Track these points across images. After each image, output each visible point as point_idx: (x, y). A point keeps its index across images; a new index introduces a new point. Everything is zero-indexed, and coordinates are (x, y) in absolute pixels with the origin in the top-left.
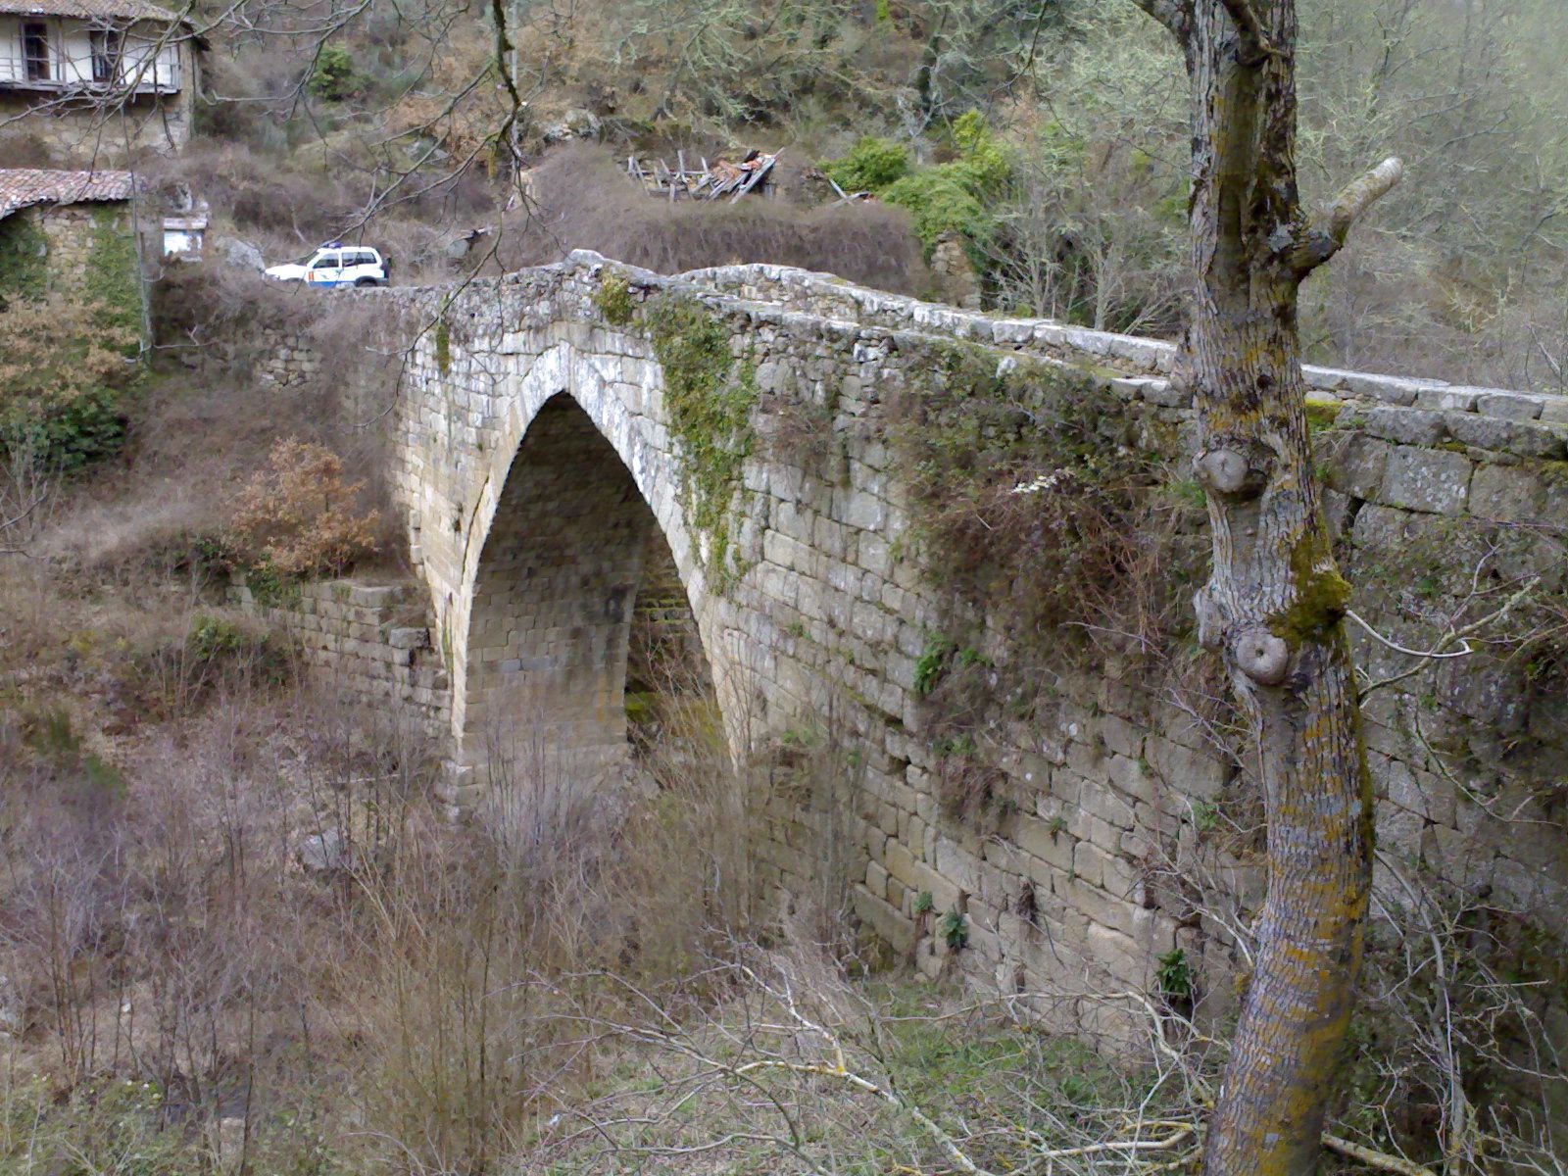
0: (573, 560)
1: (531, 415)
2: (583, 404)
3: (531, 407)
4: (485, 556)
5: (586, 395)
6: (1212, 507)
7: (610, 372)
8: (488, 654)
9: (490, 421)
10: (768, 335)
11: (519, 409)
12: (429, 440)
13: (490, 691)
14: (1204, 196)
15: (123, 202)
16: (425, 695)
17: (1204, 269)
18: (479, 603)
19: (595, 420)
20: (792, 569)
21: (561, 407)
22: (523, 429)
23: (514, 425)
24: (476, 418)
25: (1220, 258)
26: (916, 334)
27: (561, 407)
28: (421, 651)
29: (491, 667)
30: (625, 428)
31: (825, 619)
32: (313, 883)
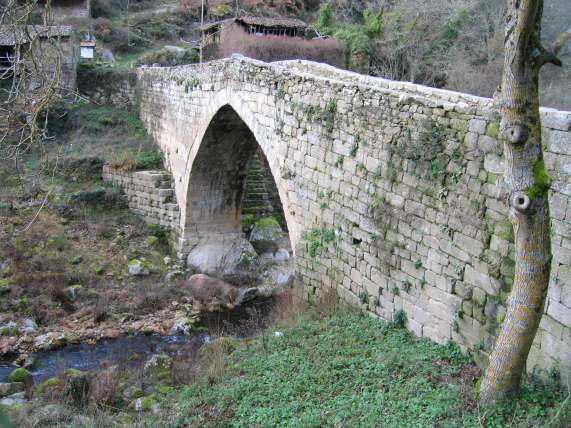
0: (225, 165)
1: (215, 113)
2: (235, 108)
3: (214, 110)
4: (194, 164)
5: (236, 107)
6: (505, 146)
7: (246, 97)
8: (196, 199)
9: (198, 114)
10: (308, 84)
11: (209, 111)
12: (174, 120)
13: (194, 213)
14: (511, 37)
15: (68, 37)
16: (171, 213)
17: (511, 61)
18: (193, 180)
19: (240, 115)
20: (316, 169)
21: (226, 111)
22: (211, 118)
23: (208, 116)
24: (193, 114)
25: (517, 59)
26: (141, 58)
27: (226, 111)
28: (170, 198)
29: (195, 203)
30: (251, 117)
31: (504, 254)
32: (181, 394)
